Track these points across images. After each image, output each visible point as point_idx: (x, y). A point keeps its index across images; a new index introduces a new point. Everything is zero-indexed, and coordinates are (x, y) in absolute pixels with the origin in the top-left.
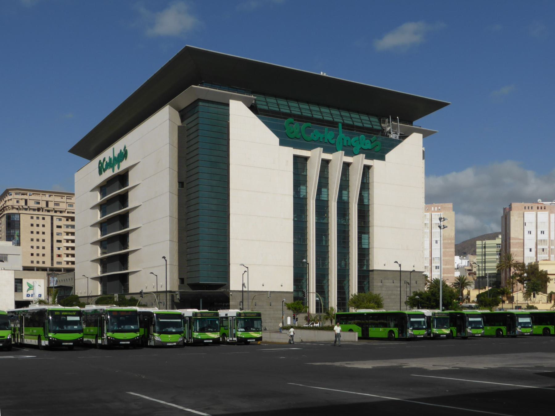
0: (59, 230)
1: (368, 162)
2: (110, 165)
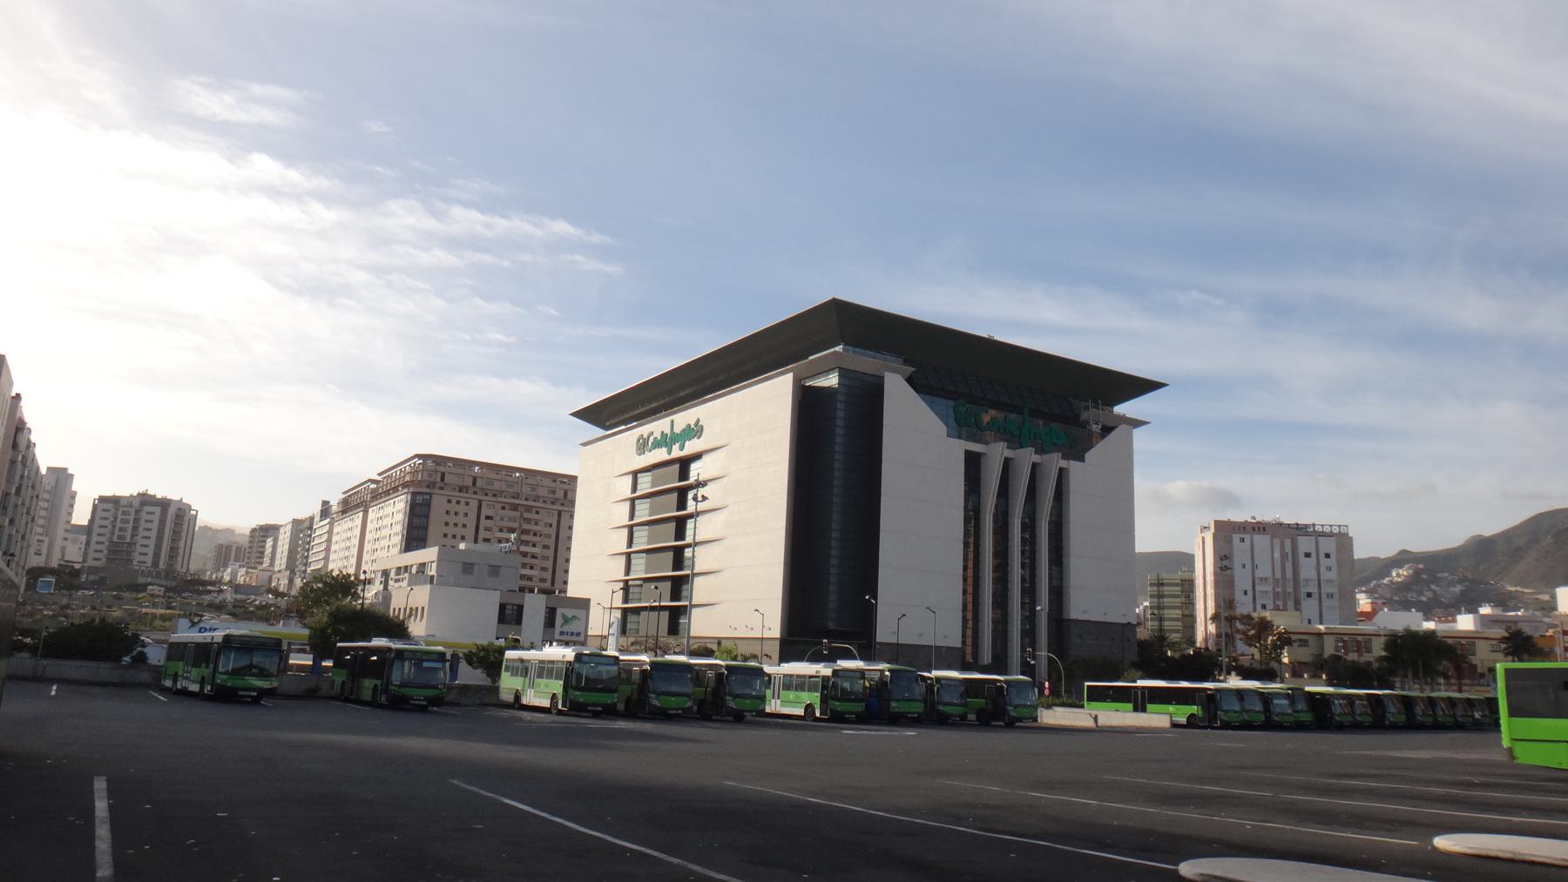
0: (489, 523)
1: (1063, 464)
2: (666, 441)
